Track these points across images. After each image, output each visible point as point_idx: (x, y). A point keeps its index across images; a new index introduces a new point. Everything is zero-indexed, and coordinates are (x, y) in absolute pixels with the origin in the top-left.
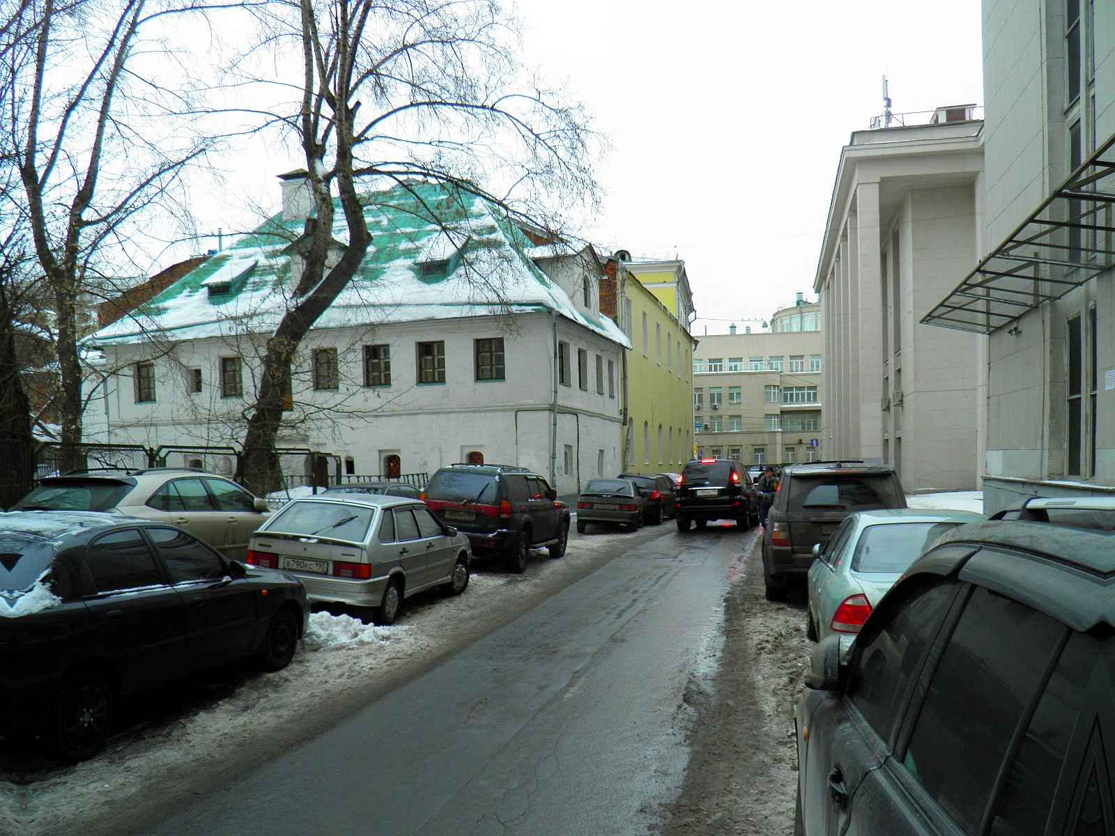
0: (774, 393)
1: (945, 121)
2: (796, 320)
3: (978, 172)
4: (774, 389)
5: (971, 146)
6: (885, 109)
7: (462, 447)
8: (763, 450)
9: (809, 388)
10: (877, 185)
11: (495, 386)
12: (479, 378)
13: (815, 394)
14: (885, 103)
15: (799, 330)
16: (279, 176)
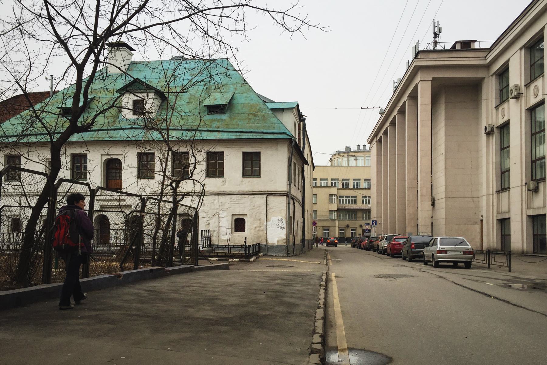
0: (335, 198)
1: (460, 48)
2: (345, 159)
3: (484, 78)
4: (334, 197)
5: (482, 62)
6: (434, 39)
7: (233, 215)
8: (328, 230)
9: (353, 197)
10: (430, 82)
11: (255, 180)
12: (244, 175)
13: (356, 201)
14: (433, 36)
15: (347, 165)
16: (135, 51)
